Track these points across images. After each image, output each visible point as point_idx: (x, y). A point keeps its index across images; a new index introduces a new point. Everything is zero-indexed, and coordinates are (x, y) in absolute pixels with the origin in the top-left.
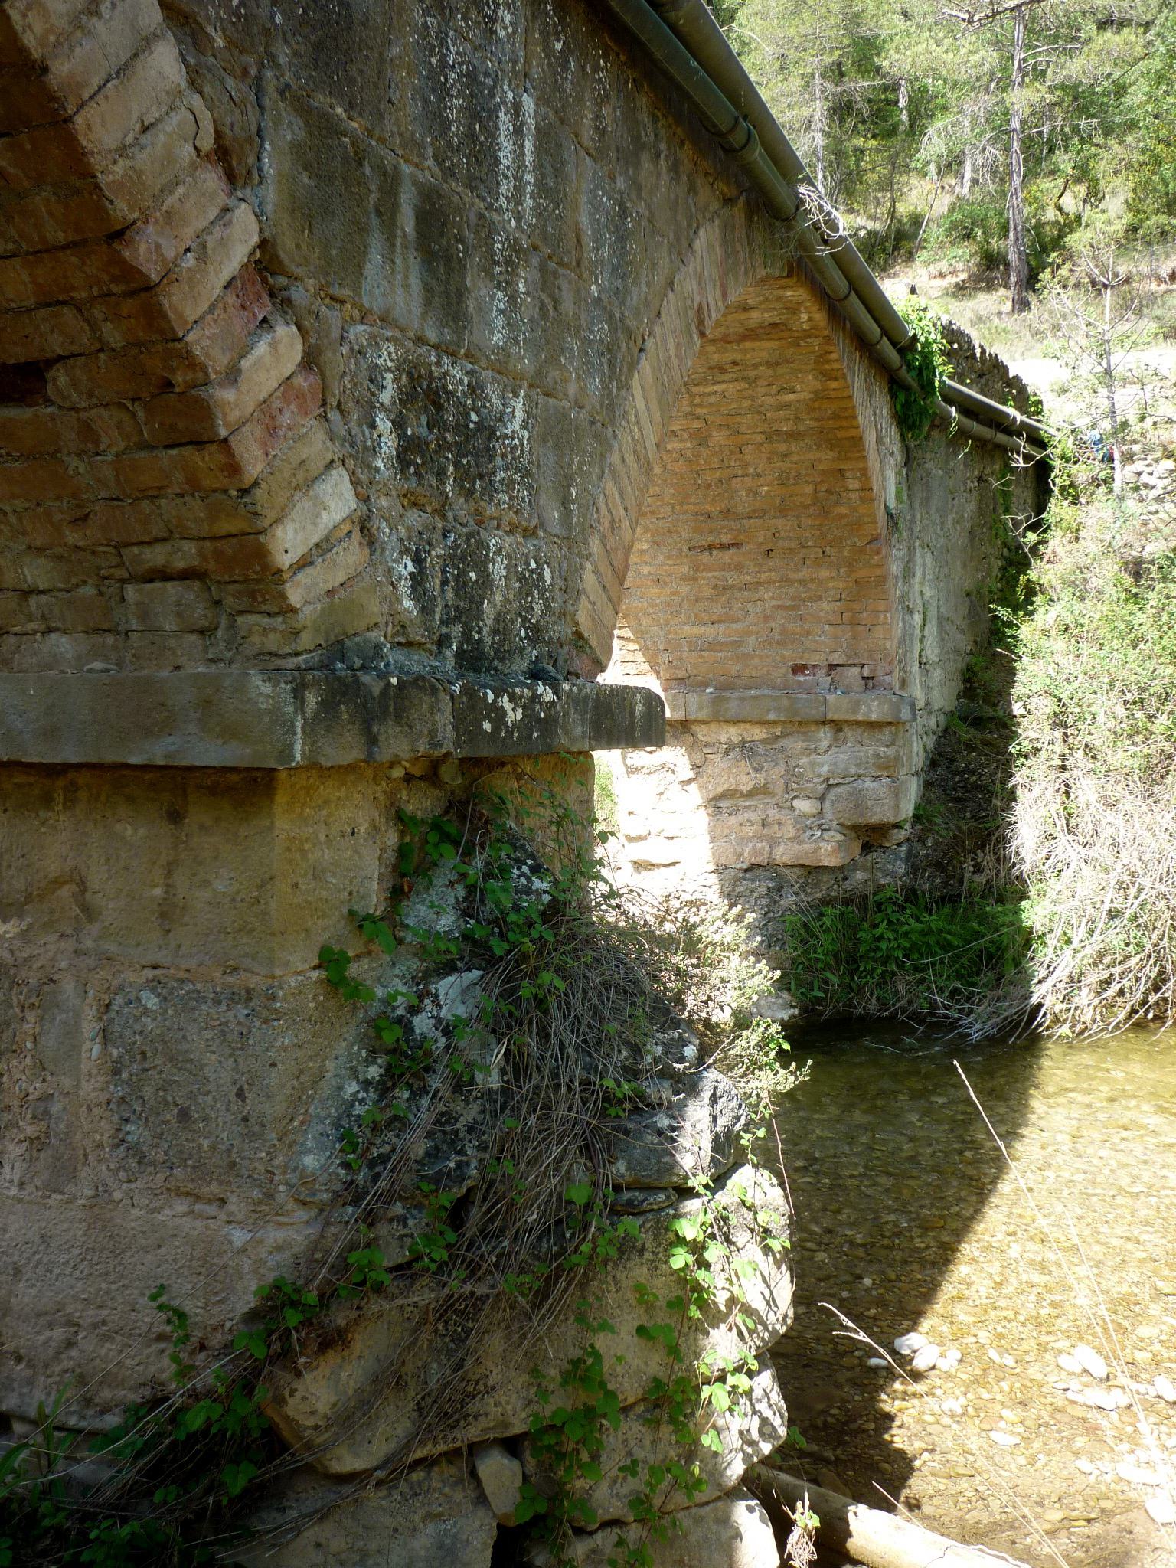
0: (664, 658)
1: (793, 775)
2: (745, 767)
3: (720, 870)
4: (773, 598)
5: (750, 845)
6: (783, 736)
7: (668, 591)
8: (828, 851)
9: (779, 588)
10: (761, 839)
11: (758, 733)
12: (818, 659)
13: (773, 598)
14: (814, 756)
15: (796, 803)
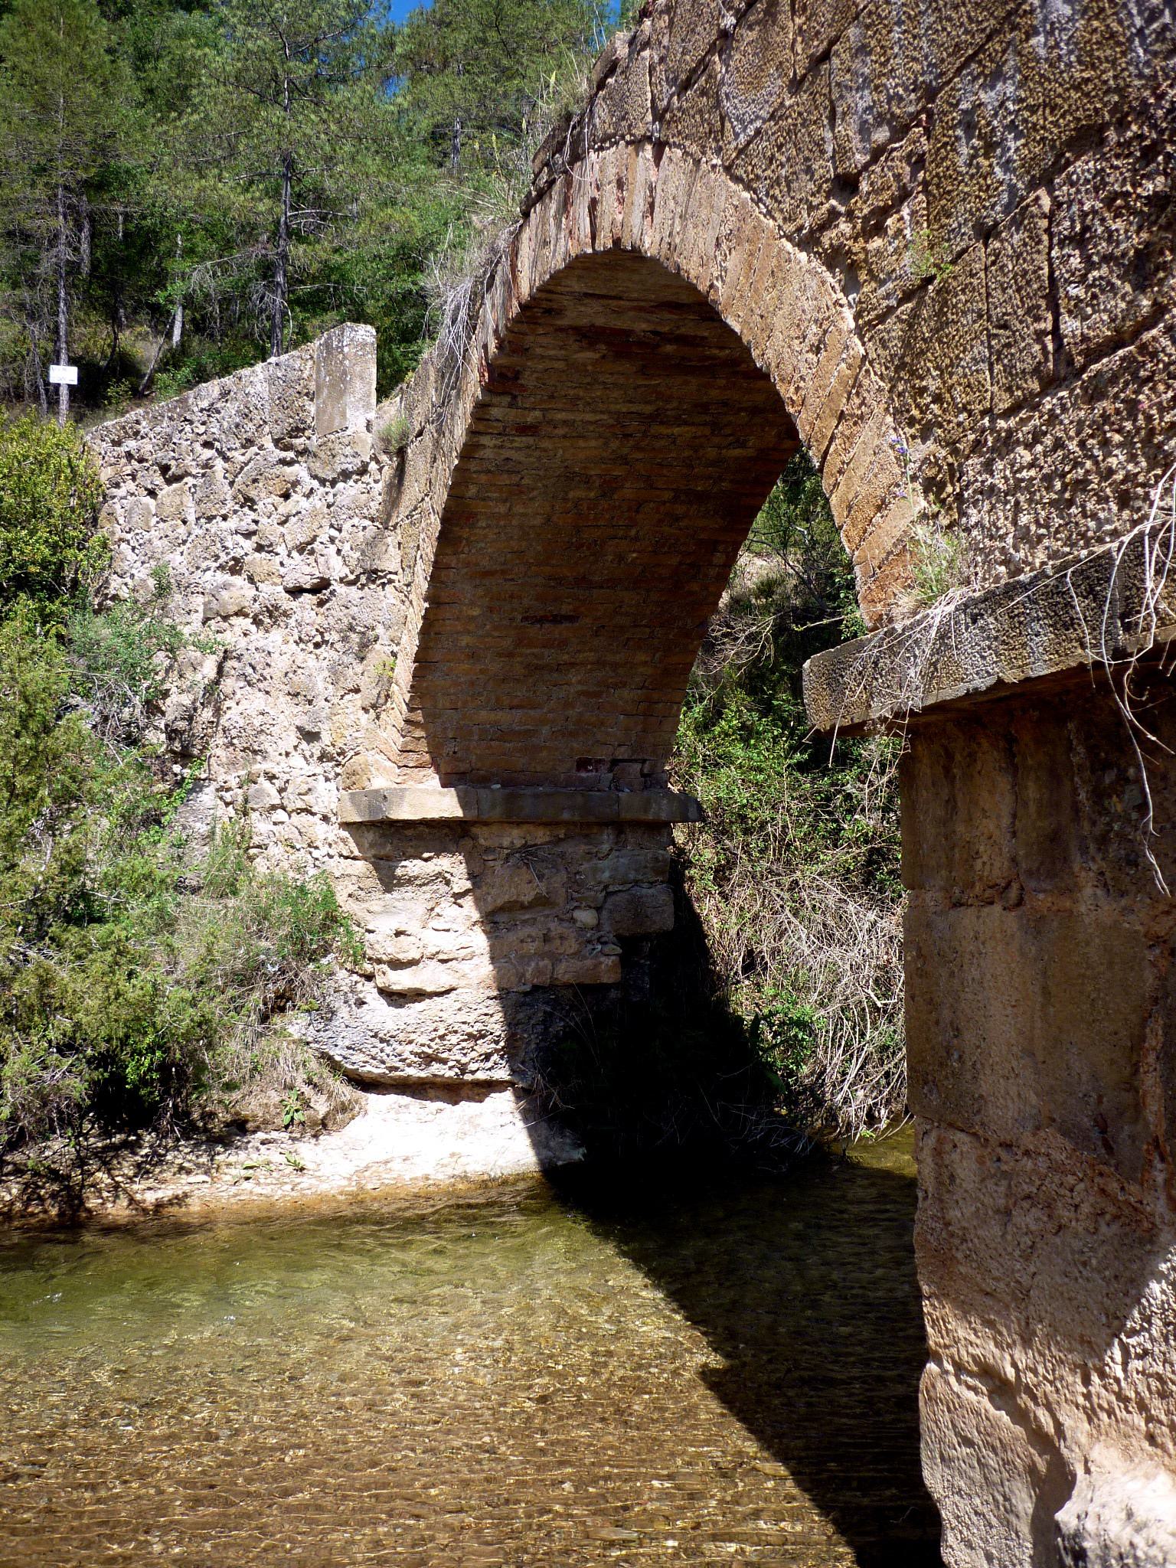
0: (450, 748)
1: (574, 882)
2: (525, 874)
3: (503, 995)
4: (579, 682)
5: (533, 964)
6: (567, 837)
7: (479, 667)
8: (606, 966)
9: (591, 671)
10: (542, 956)
11: (541, 836)
12: (603, 754)
13: (579, 682)
14: (595, 861)
15: (577, 914)
